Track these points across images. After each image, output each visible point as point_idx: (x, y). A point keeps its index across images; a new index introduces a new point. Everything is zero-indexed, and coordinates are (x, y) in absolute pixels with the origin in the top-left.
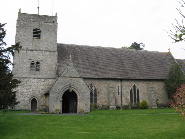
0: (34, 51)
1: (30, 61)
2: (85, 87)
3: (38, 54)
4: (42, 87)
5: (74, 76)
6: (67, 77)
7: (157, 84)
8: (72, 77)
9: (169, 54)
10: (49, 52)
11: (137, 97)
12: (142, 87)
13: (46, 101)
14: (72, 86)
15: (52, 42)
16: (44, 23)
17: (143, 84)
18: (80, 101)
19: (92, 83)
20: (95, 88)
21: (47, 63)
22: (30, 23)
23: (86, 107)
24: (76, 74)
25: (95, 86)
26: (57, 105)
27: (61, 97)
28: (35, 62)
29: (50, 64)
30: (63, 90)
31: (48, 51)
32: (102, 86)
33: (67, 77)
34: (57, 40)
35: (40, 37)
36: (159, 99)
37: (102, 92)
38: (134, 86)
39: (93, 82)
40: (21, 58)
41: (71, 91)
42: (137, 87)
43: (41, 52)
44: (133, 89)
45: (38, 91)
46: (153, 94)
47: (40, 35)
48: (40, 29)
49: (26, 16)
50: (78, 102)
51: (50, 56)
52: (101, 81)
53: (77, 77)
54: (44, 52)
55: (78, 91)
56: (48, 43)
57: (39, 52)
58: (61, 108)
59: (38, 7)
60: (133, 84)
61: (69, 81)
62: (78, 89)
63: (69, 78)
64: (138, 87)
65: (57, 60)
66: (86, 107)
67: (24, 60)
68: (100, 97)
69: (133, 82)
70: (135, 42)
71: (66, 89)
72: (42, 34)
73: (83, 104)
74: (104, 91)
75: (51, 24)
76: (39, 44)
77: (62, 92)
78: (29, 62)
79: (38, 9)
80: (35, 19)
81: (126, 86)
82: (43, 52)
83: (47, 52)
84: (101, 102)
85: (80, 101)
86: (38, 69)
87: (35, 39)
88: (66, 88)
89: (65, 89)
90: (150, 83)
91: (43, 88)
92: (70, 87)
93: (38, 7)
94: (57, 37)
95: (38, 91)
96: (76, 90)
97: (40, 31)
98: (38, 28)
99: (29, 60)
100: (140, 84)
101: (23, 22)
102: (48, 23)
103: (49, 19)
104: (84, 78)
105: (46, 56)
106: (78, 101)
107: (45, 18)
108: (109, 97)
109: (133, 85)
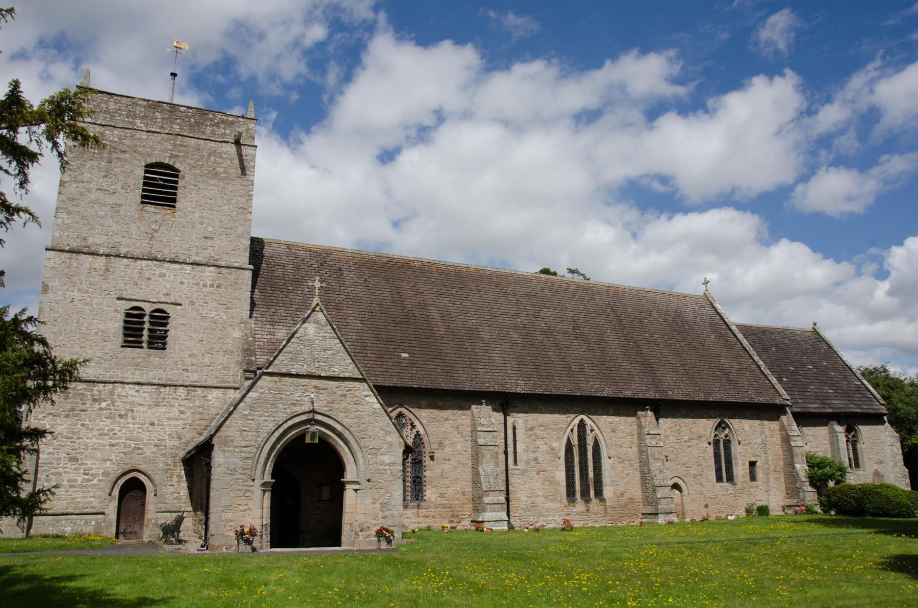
3: (164, 275)
4: (177, 423)
11: (591, 475)
12: (613, 431)
18: (357, 487)
20: (418, 434)
21: (204, 318)
22: (132, 136)
24: (345, 366)
25: (416, 423)
28: (148, 308)
35: (174, 201)
36: (680, 482)
40: (79, 291)
41: (317, 441)
44: (575, 441)
47: (175, 194)
48: (177, 166)
49: (112, 106)
51: (219, 286)
56: (210, 229)
57: (167, 265)
62: (347, 434)
68: (439, 471)
72: (185, 188)
73: (368, 503)
78: (116, 311)
85: (357, 487)
86: (158, 341)
95: (156, 445)
97: (177, 176)
98: (166, 161)
105: (198, 284)
109: (577, 421)
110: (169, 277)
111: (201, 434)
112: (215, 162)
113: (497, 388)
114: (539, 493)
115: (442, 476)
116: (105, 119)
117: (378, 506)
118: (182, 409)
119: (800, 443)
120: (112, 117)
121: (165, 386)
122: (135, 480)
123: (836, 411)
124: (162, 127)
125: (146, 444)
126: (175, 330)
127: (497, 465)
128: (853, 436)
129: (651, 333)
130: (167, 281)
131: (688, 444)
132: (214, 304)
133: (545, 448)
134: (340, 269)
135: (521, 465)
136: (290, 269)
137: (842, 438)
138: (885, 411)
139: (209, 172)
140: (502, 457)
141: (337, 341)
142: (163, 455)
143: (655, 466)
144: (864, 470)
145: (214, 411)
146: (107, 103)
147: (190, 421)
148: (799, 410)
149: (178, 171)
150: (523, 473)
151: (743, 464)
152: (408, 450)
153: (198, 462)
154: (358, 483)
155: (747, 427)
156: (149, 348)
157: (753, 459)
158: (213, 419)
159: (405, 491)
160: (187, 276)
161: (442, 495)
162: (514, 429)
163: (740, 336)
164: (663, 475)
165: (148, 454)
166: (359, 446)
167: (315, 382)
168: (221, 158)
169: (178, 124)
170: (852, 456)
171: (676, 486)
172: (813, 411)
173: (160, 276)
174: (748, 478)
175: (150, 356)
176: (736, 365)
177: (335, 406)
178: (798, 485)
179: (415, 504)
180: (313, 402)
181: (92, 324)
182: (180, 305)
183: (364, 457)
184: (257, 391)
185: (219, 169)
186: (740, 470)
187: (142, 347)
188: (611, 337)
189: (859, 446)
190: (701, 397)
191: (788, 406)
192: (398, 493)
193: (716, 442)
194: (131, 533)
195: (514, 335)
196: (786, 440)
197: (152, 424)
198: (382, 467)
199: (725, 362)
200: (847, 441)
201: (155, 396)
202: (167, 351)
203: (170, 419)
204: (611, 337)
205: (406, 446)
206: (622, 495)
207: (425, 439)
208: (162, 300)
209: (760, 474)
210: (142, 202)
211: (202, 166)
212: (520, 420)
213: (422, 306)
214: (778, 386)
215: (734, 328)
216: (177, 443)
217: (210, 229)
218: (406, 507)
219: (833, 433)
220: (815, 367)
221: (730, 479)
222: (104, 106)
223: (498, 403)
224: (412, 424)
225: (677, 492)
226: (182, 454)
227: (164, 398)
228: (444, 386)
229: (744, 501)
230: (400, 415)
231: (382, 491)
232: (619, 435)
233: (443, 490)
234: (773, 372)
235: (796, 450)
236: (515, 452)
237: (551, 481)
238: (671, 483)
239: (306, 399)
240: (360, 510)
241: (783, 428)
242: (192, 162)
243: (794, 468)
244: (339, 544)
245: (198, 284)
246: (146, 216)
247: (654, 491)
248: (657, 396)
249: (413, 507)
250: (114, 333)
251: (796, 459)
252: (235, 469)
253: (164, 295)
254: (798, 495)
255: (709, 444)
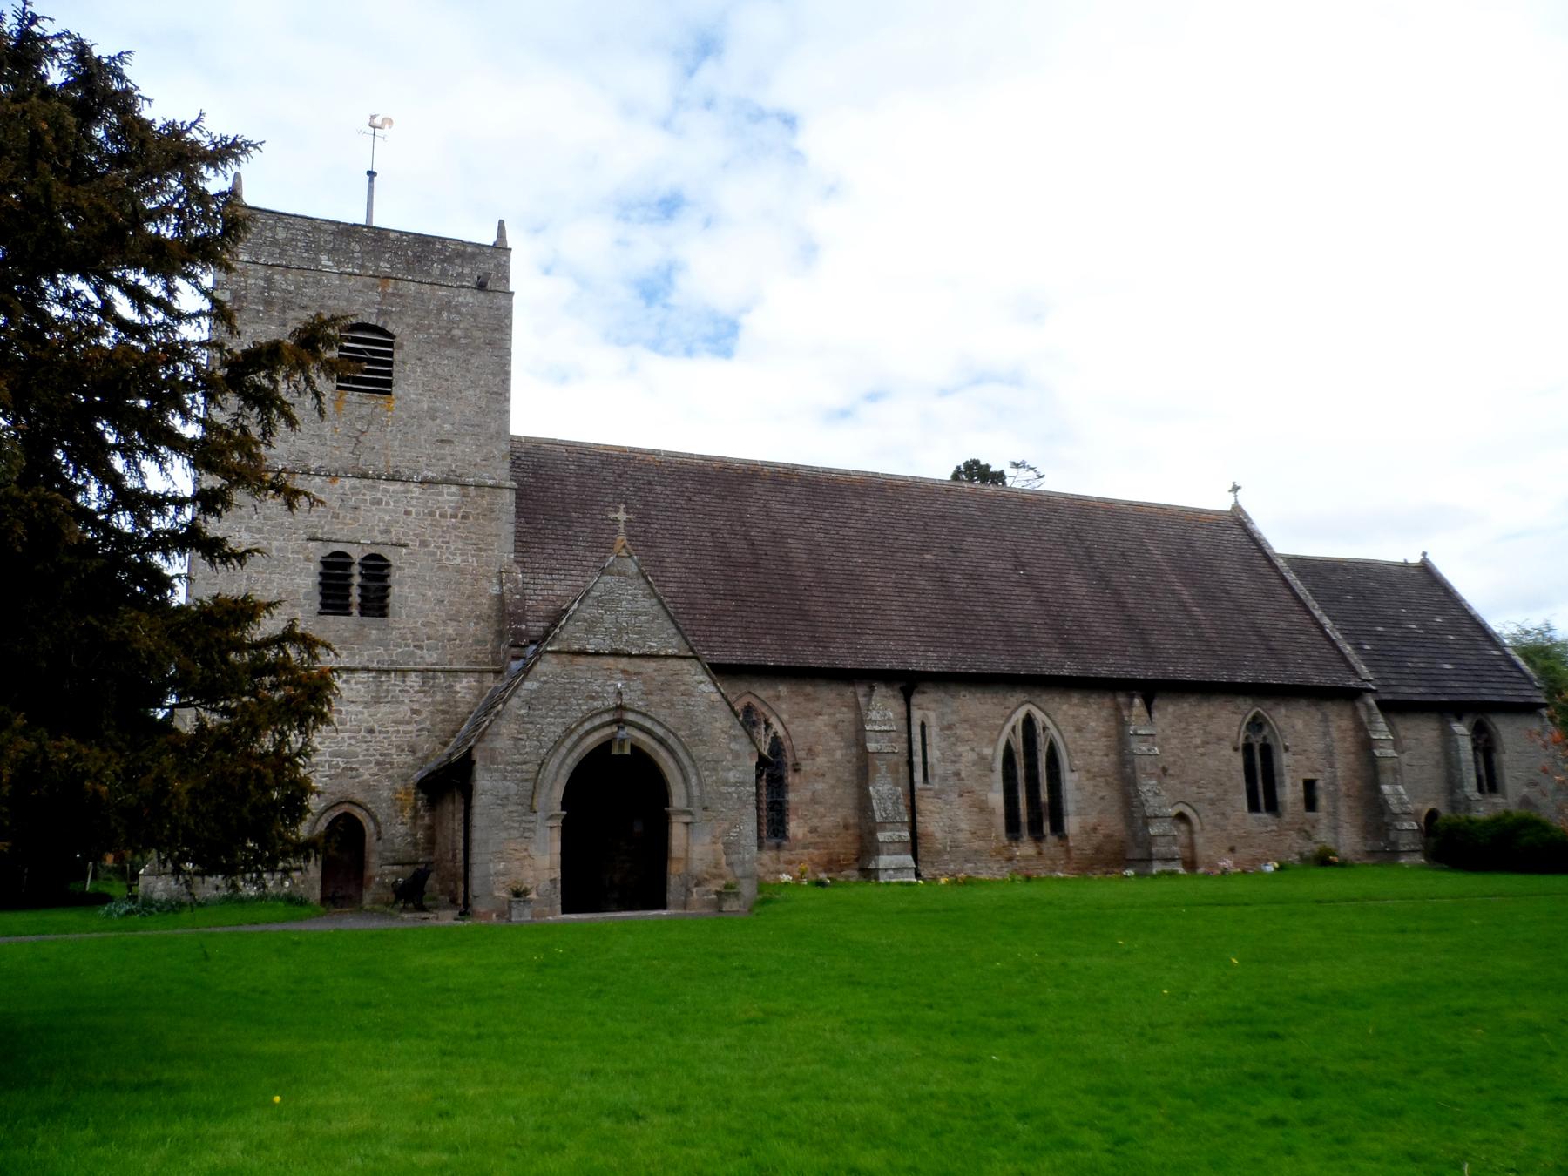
0: (347, 483)
1: (319, 551)
2: (721, 725)
3: (379, 502)
4: (409, 728)
5: (645, 650)
6: (597, 654)
7: (1171, 709)
8: (630, 655)
9: (1237, 522)
10: (454, 489)
11: (1044, 796)
12: (1079, 729)
13: (430, 828)
14: (630, 717)
15: (476, 421)
16: (412, 287)
17: (1085, 712)
18: (688, 819)
19: (755, 702)
20: (775, 738)
21: (442, 567)
22: (317, 283)
23: (730, 864)
24: (664, 638)
25: (773, 720)
26: (523, 850)
27: (558, 793)
28: (357, 554)
29: (460, 571)
30: (568, 743)
31: (445, 482)
32: (820, 723)
33: (597, 654)
34: (508, 412)
35: (389, 384)
36: (1188, 811)
37: (822, 760)
38: (1029, 722)
39: (760, 693)
40: (248, 529)
41: (627, 751)
42: (1045, 729)
43: (398, 486)
44: (1018, 745)
45: (378, 763)
46: (1150, 775)
47: (389, 373)
48: (390, 328)
49: (281, 235)
50: (678, 833)
51: (465, 517)
52: (809, 689)
53: (667, 657)
54: (416, 490)
55: (672, 752)
56: (447, 427)
57: (383, 485)
58: (558, 874)
59: (371, 174)
60: (1018, 707)
61: (610, 683)
62: (671, 740)
63: (611, 661)
64: (1052, 730)
65: (510, 547)
66: (730, 864)
67: (275, 544)
68: (809, 794)
69: (1020, 696)
70: (976, 462)
71: (592, 741)
72: (404, 363)
73: (707, 837)
74: (830, 752)
75: (467, 298)
76: (383, 426)
77: (565, 758)
78: (307, 559)
79: (371, 181)
80: (349, 254)
81: (973, 724)
82: (412, 486)
83: (445, 489)
84: (813, 830)
85: (688, 819)
86: (376, 603)
87: (354, 397)
88: (588, 733)
89: (581, 738)
90: (1130, 706)
91: (412, 738)
92: (620, 722)
93: (371, 174)
94: (508, 390)
95: (378, 763)
96: (661, 741)
97: (390, 345)
98: (373, 321)
99: (312, 539)
100: (1065, 714)
101: (262, 272)
102: (443, 292)
103: (449, 260)
104: (720, 671)
105: (432, 514)
106: (674, 819)
107: (423, 252)
108: (869, 797)
109: (1020, 714)
110: (388, 503)
111: (445, 744)
112: (450, 321)
113: (895, 664)
114: (963, 826)
115: (814, 800)
116: (271, 255)
117: (720, 846)
118: (415, 706)
119: (1390, 752)
120: (282, 253)
121: (388, 672)
122: (347, 816)
123: (1455, 698)
124: (362, 266)
125: (361, 763)
126: (401, 590)
127: (897, 784)
128: (1487, 741)
129: (1141, 574)
130: (385, 511)
131: (1201, 750)
132: (460, 544)
133: (972, 756)
134: (650, 483)
135: (935, 784)
136: (571, 484)
137: (1466, 746)
138: (1543, 700)
139: (441, 337)
140: (903, 769)
141: (654, 601)
142: (390, 777)
143: (1147, 786)
144: (1504, 797)
145: (463, 709)
146: (273, 229)
147: (427, 724)
148: (1389, 697)
149: (393, 337)
150: (937, 796)
151: (1294, 785)
152: (762, 762)
153: (448, 783)
154: (690, 813)
155: (1299, 725)
156: (362, 614)
157: (1310, 776)
158: (464, 720)
159: (759, 823)
160: (414, 502)
161: (813, 830)
162: (923, 726)
163: (1291, 577)
164: (1157, 797)
165: (366, 777)
166: (690, 757)
167: (623, 663)
168: (459, 313)
169: (388, 261)
170: (1483, 772)
171: (1182, 817)
172: (1416, 698)
173: (372, 504)
174: (1301, 807)
175: (363, 626)
176: (1282, 624)
177: (656, 698)
178: (1386, 819)
179: (773, 842)
180: (620, 693)
181: (271, 581)
182: (405, 546)
183: (698, 775)
184: (537, 680)
185: (456, 332)
186: (1290, 793)
187: (350, 614)
188: (1078, 585)
189: (1496, 758)
190: (1223, 676)
191: (1370, 691)
192: (749, 827)
193: (1248, 749)
194: (343, 898)
195: (921, 581)
196: (1366, 745)
197: (371, 731)
198: (724, 789)
199: (1262, 620)
200: (1475, 749)
201: (373, 687)
202: (390, 619)
203: (397, 722)
204: (1078, 585)
205: (761, 756)
206: (1095, 829)
207: (787, 744)
208: (379, 540)
209: (1323, 802)
210: (339, 388)
211: (430, 326)
212: (930, 708)
213: (777, 537)
214: (1354, 658)
215: (1280, 563)
216: (409, 759)
217: (447, 427)
218: (760, 847)
219: (1448, 737)
220: (1422, 626)
221: (1273, 806)
222: (268, 234)
223: (897, 686)
224: (766, 722)
225: (1183, 827)
226: (417, 775)
227: (388, 691)
228: (814, 663)
229: (1294, 845)
230: (749, 709)
231: (726, 825)
232: (1089, 736)
233: (815, 822)
234: (1347, 636)
235: (1381, 763)
236: (925, 763)
237: (983, 808)
238: (1173, 811)
239: (611, 689)
240: (693, 846)
241: (1361, 727)
242: (412, 321)
243: (1379, 791)
244: (664, 907)
245: (432, 514)
246: (345, 407)
247: (1146, 825)
248: (1150, 675)
249: (770, 849)
250: (306, 594)
251: (1382, 778)
252: (507, 798)
253: (381, 532)
254: (1387, 836)
255: (1236, 749)
